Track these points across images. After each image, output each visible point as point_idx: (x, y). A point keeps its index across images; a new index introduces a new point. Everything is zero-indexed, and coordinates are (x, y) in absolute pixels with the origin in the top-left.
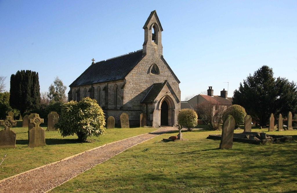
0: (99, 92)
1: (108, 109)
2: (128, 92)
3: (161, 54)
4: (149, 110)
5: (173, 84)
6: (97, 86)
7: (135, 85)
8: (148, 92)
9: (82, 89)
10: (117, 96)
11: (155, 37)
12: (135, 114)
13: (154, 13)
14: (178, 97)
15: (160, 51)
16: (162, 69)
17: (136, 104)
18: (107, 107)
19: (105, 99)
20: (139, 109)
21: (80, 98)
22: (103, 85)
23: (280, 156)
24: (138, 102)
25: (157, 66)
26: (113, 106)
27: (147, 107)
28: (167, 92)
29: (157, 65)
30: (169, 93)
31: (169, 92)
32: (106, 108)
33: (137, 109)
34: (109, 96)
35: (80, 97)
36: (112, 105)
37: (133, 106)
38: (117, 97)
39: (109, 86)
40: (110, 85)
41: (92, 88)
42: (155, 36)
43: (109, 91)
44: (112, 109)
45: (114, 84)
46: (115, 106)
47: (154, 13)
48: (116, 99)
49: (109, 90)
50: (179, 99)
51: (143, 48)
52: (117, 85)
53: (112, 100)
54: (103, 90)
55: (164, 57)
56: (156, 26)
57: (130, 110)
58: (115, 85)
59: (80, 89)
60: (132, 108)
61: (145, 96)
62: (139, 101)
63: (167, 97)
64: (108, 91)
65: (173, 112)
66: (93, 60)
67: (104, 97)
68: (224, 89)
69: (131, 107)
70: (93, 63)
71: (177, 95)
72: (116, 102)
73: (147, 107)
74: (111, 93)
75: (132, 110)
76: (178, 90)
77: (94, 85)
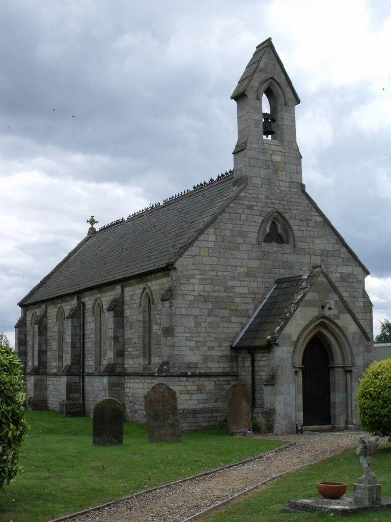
0: (99, 318)
1: (124, 374)
2: (184, 311)
3: (299, 181)
4: (261, 373)
5: (344, 278)
6: (93, 298)
7: (209, 288)
8: (256, 308)
9: (53, 311)
10: (150, 327)
11: (270, 125)
12: (212, 387)
13: (267, 48)
14: (362, 323)
15: (293, 167)
16: (304, 229)
17: (213, 353)
18: (124, 364)
19: (116, 338)
20: (227, 370)
21: (46, 340)
22: (109, 293)
23: (376, 447)
24: (222, 346)
25: (283, 218)
26: (141, 361)
27: (253, 361)
28: (323, 307)
29: (287, 216)
30: (330, 309)
31: (328, 306)
32: (118, 370)
33: (220, 370)
34: (127, 327)
35: (48, 334)
36: (137, 357)
37: (206, 359)
38: (150, 331)
39: (126, 294)
40: (128, 291)
41: (79, 305)
42: (273, 120)
43: (127, 312)
44: (137, 370)
45: (142, 286)
46: (147, 362)
47: (267, 48)
48: (150, 337)
49: (126, 307)
50: (368, 331)
51: (235, 165)
52: (151, 291)
53: (136, 340)
54: (108, 310)
55: (307, 190)
56: (276, 88)
57: (193, 375)
58: (145, 289)
59: (48, 311)
60: (199, 366)
61: (245, 324)
62: (225, 340)
63: (324, 322)
64: (122, 311)
65: (349, 376)
66: (92, 221)
67: (111, 333)
68: (92, 217)
69: (197, 363)
70: (92, 230)
71: (359, 316)
72: (150, 349)
73: (253, 361)
74: (134, 318)
75: (200, 375)
76: (362, 300)
77: (83, 294)
